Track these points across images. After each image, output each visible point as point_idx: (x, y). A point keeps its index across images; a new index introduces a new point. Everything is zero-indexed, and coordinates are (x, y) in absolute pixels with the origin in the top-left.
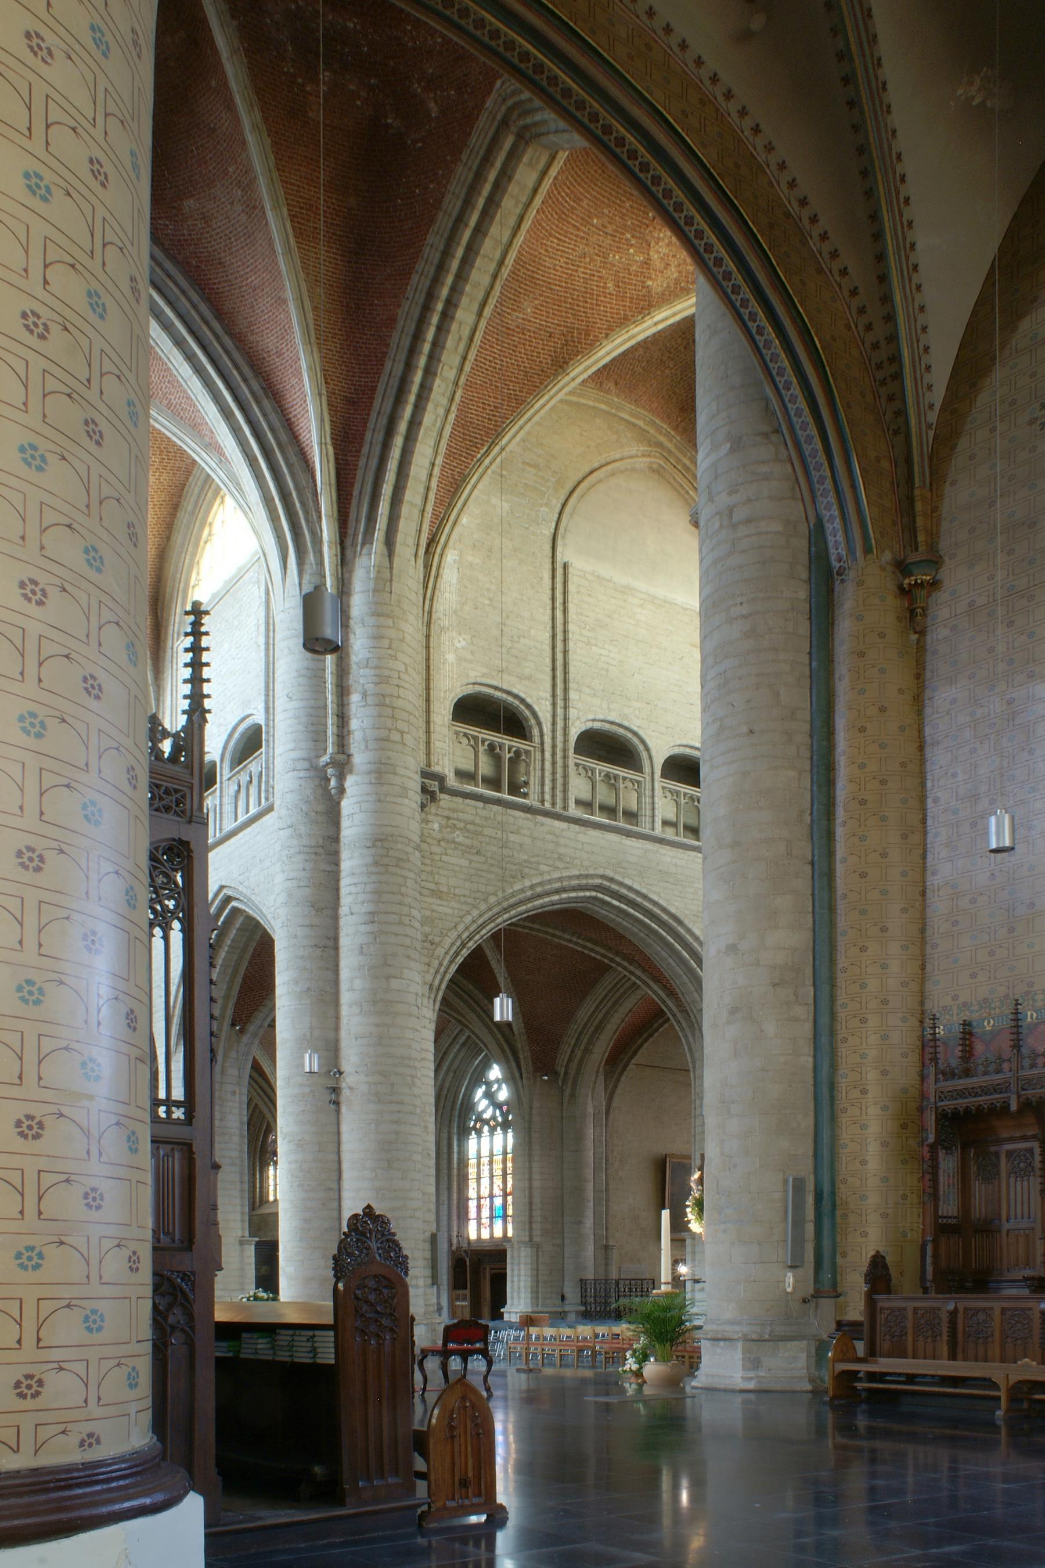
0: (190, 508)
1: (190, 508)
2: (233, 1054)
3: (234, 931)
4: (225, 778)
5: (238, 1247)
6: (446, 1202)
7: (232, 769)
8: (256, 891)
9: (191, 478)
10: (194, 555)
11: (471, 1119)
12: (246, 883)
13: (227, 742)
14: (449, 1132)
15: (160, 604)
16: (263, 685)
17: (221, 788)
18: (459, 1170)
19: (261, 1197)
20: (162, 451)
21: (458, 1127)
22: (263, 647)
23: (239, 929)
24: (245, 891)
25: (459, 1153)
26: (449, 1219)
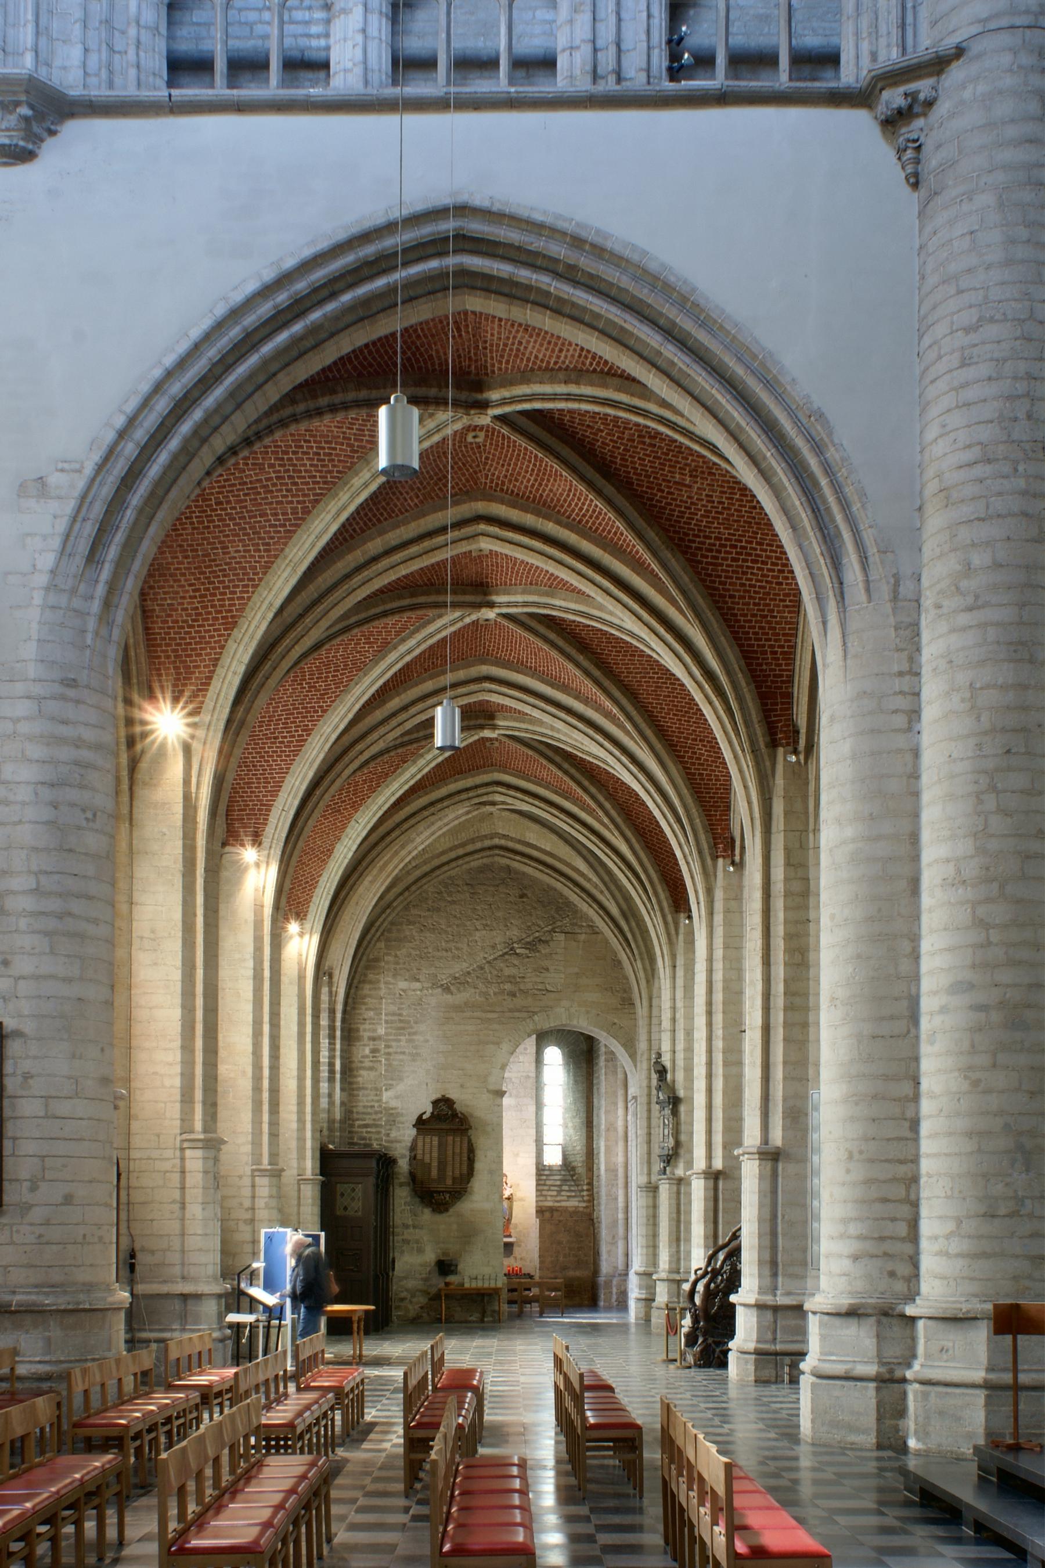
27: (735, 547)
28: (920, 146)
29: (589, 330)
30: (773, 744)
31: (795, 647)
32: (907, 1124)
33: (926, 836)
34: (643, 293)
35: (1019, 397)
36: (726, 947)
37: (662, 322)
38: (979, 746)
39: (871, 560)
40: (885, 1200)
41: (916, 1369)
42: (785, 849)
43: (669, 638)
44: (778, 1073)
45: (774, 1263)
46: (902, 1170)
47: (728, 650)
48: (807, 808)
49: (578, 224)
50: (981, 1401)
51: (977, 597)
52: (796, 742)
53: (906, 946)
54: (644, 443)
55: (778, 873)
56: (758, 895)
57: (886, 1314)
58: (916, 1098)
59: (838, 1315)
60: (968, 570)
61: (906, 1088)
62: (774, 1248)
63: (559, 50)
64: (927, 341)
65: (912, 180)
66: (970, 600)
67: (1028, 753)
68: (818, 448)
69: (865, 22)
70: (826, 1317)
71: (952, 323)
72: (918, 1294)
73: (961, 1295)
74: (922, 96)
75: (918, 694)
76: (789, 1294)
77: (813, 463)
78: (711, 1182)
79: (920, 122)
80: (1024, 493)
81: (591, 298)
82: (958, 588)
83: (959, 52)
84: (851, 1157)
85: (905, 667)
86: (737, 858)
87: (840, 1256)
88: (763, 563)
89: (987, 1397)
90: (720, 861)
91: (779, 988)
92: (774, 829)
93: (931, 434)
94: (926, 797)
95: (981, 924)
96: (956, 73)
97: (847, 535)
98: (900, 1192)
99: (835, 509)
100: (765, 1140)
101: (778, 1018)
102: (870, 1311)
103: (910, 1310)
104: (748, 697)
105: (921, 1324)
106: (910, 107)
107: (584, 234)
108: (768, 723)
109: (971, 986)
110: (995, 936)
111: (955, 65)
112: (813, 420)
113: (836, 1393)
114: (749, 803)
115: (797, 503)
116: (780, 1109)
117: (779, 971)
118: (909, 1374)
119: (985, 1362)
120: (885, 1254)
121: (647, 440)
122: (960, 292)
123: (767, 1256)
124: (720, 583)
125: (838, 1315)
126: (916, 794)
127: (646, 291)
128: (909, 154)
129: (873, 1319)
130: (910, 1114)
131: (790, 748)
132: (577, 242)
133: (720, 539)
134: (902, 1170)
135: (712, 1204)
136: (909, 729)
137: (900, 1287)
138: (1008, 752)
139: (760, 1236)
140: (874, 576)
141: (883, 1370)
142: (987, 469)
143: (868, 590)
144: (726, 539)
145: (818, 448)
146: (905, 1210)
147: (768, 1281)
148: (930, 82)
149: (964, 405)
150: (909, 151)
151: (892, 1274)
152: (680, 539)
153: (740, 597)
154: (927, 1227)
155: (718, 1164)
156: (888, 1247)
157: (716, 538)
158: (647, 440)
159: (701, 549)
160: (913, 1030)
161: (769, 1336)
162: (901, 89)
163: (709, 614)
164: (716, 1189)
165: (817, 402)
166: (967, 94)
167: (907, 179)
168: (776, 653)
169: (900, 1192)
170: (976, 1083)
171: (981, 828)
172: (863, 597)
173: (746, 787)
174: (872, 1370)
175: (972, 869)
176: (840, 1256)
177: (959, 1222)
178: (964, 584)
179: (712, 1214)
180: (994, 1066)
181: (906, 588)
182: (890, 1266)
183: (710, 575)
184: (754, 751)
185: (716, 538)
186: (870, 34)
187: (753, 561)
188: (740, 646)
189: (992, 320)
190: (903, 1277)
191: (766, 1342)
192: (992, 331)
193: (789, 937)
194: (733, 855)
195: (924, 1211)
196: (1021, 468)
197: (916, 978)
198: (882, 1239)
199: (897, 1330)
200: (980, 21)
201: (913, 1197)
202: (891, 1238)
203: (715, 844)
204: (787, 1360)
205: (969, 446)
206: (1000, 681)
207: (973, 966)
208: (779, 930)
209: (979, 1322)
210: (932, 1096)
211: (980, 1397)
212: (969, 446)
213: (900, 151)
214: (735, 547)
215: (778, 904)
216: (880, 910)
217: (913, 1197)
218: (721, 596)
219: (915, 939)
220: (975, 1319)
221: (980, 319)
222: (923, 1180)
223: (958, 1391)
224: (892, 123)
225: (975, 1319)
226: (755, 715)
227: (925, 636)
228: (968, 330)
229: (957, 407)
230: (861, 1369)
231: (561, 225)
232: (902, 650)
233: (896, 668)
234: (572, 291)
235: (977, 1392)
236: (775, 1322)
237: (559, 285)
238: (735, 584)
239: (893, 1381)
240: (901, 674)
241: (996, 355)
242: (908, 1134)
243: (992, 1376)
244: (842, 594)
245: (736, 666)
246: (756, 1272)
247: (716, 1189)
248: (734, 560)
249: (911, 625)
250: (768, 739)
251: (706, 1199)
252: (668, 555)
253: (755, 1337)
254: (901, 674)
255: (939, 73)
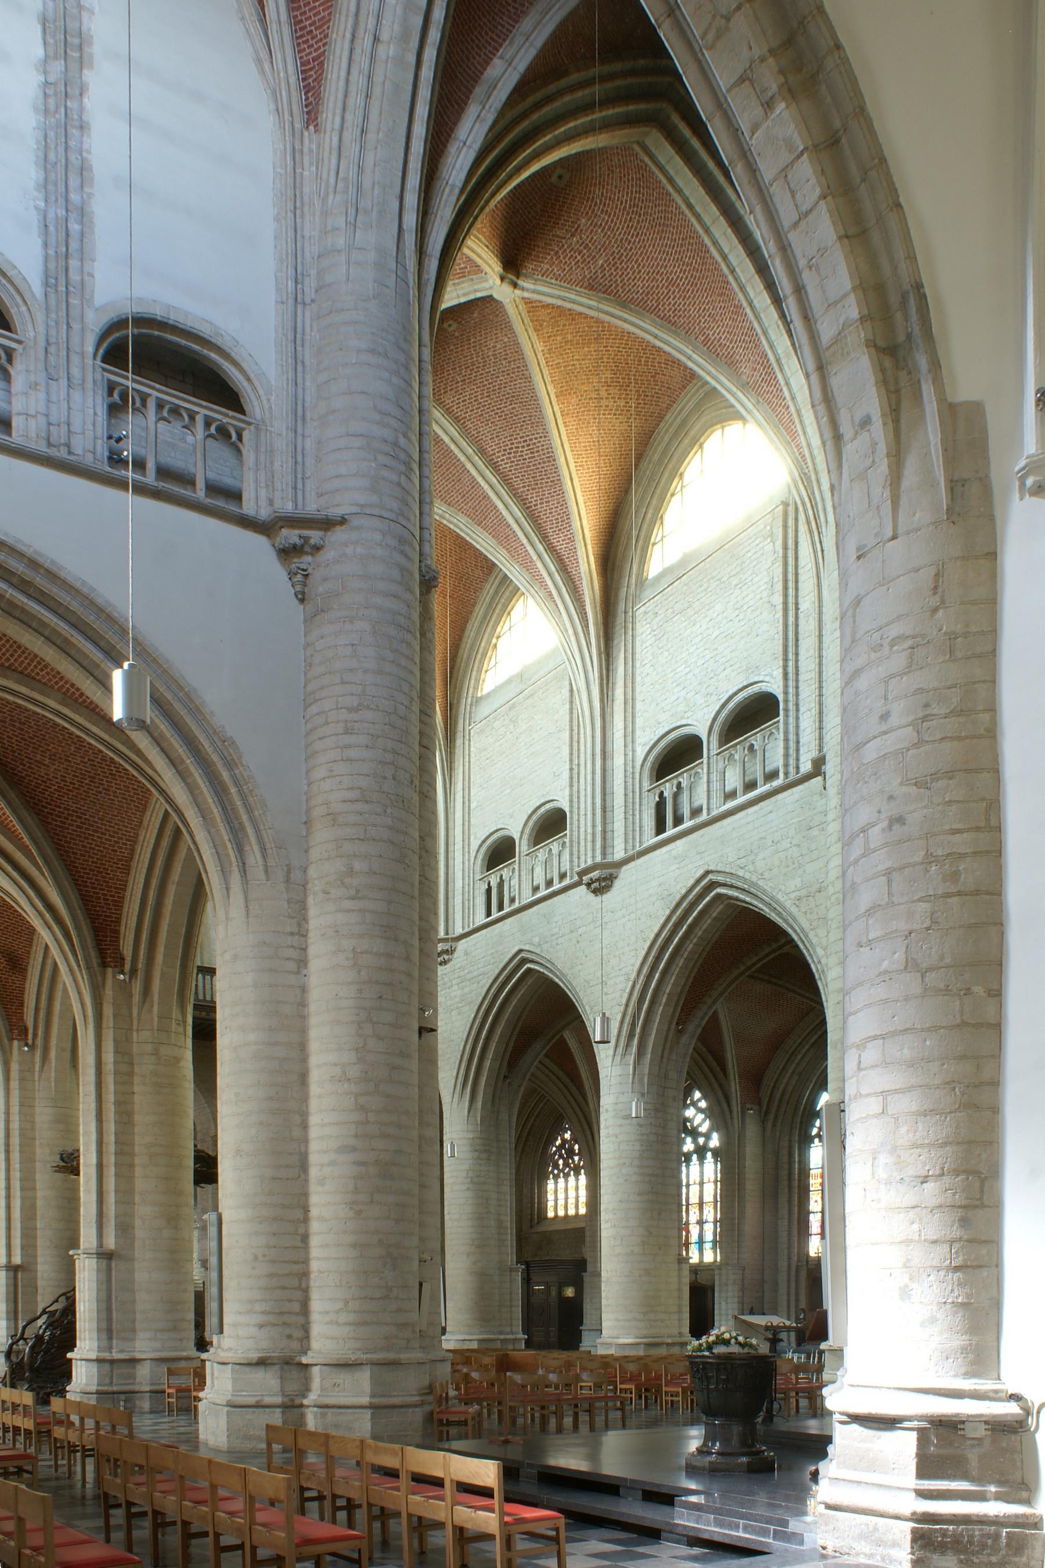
0: (656, 457)
1: (656, 457)
2: (674, 1057)
3: (709, 921)
4: (712, 753)
5: (676, 1265)
6: (786, 1217)
7: (721, 744)
8: (766, 875)
9: (662, 425)
10: (658, 509)
11: (814, 1126)
12: (751, 868)
13: (718, 713)
14: (790, 1141)
15: (610, 564)
16: (780, 648)
17: (709, 763)
18: (799, 1180)
19: (539, 1213)
20: (639, 395)
21: (800, 1135)
22: (780, 607)
23: (715, 919)
24: (747, 876)
25: (800, 1162)
26: (790, 1234)
27: (81, 818)
28: (307, 575)
29: (35, 634)
30: (104, 965)
31: (123, 898)
32: (299, 1238)
33: (314, 1046)
34: (91, 618)
35: (388, 763)
36: (21, 1105)
37: (102, 644)
38: (360, 991)
39: (269, 851)
40: (284, 1288)
41: (312, 1398)
42: (115, 1040)
43: (15, 874)
44: (111, 1198)
45: (109, 1332)
46: (296, 1268)
47: (70, 892)
48: (131, 1014)
49: (35, 551)
50: (369, 1416)
51: (358, 891)
52: (123, 965)
53: (297, 1119)
54: (14, 726)
55: (109, 1057)
56: (92, 1071)
57: (287, 1363)
58: (306, 1220)
59: (249, 1364)
60: (351, 872)
61: (298, 1214)
62: (109, 1319)
63: (14, 412)
64: (314, 709)
65: (300, 596)
66: (353, 892)
67: (393, 1000)
68: (230, 765)
69: (262, 477)
70: (238, 1367)
71: (337, 702)
72: (309, 1349)
73: (349, 1349)
74: (312, 542)
75: (305, 950)
76: (122, 1351)
77: (225, 775)
78: (12, 1274)
79: (309, 558)
80: (390, 828)
81: (42, 611)
82: (343, 883)
83: (343, 521)
84: (256, 1258)
85: (295, 930)
86: (30, 1042)
87: (248, 1325)
88: (102, 833)
89: (372, 1414)
90: (16, 1043)
91: (110, 1138)
92: (104, 1026)
93: (319, 773)
94: (313, 1020)
95: (361, 1108)
96: (338, 535)
97: (250, 831)
98: (295, 1282)
99: (242, 811)
100: (100, 1244)
101: (110, 1159)
102: (275, 1361)
103: (305, 1360)
104: (84, 927)
105: (316, 1370)
106: (302, 546)
107: (41, 560)
108: (100, 949)
109: (354, 1149)
110: (372, 1117)
111: (338, 528)
112: (224, 743)
113: (248, 1417)
114: (83, 1004)
115: (210, 801)
116: (113, 1223)
117: (110, 1127)
118: (305, 1402)
119: (369, 1391)
120: (284, 1324)
121: (17, 725)
122: (343, 683)
123: (104, 1325)
124: (66, 842)
125: (249, 1364)
126: (304, 1018)
127: (92, 618)
128: (299, 577)
129: (277, 1367)
130: (301, 1231)
131: (117, 970)
132: (34, 564)
133: (68, 810)
134: (296, 1268)
135: (12, 1289)
136: (298, 973)
137: (295, 1345)
138: (380, 997)
139: (98, 1311)
140: (271, 862)
141: (286, 1400)
142: (366, 807)
143: (266, 872)
144: (73, 811)
145: (230, 765)
146: (298, 1295)
147: (105, 1343)
148: (320, 533)
149: (348, 760)
150: (299, 576)
151: (289, 1337)
152: (34, 803)
153: (81, 855)
154: (317, 1305)
155: (17, 1260)
156: (286, 1318)
157: (65, 809)
158: (17, 725)
159: (52, 814)
160: (303, 1176)
161: (107, 1381)
162: (297, 532)
163: (56, 863)
164: (16, 1278)
165: (230, 732)
166: (349, 550)
167: (296, 595)
168: (108, 900)
169: (295, 1282)
170: (359, 1213)
171: (361, 1045)
172: (263, 876)
173: (79, 993)
174: (278, 1400)
175: (354, 1072)
176: (248, 1325)
177: (346, 1302)
178: (347, 880)
179: (12, 1296)
180: (372, 1202)
181: (296, 876)
182: (288, 1331)
183: (58, 835)
184: (89, 968)
185: (65, 809)
186: (267, 485)
187: (94, 831)
188: (80, 890)
189: (368, 708)
190: (298, 1339)
191: (105, 1385)
192: (368, 715)
193: (118, 1103)
194: (27, 1039)
195: (315, 1295)
196: (389, 811)
197: (305, 1141)
198: (282, 1313)
199: (294, 1373)
200: (358, 505)
201: (304, 1285)
202: (289, 1313)
203: (11, 1030)
204: (123, 1397)
205: (352, 789)
206: (375, 950)
207: (356, 1136)
208: (110, 1097)
209: (364, 1367)
210: (322, 1219)
211: (368, 1414)
212: (352, 789)
213: (291, 574)
214: (81, 818)
215: (110, 1081)
216: (277, 1093)
217: (304, 1285)
218: (66, 851)
219: (304, 1115)
220: (362, 1364)
221: (360, 704)
222: (312, 1276)
223: (349, 1411)
224: (286, 553)
225: (362, 1364)
226: (90, 942)
227: (313, 911)
228: (350, 710)
229: (342, 760)
230: (268, 1400)
231: (20, 547)
232: (293, 918)
233: (288, 929)
234: (26, 601)
235: (365, 1411)
236: (112, 1371)
237: (14, 593)
238: (77, 845)
239: (293, 1407)
240: (292, 934)
241: (371, 731)
242: (299, 1244)
243: (375, 1400)
244: (245, 871)
245: (76, 904)
246: (96, 1336)
247: (16, 1278)
248: (78, 827)
249: (299, 901)
250: (99, 961)
251: (7, 1285)
252: (25, 813)
253: (96, 1381)
254: (292, 934)
255: (326, 530)
